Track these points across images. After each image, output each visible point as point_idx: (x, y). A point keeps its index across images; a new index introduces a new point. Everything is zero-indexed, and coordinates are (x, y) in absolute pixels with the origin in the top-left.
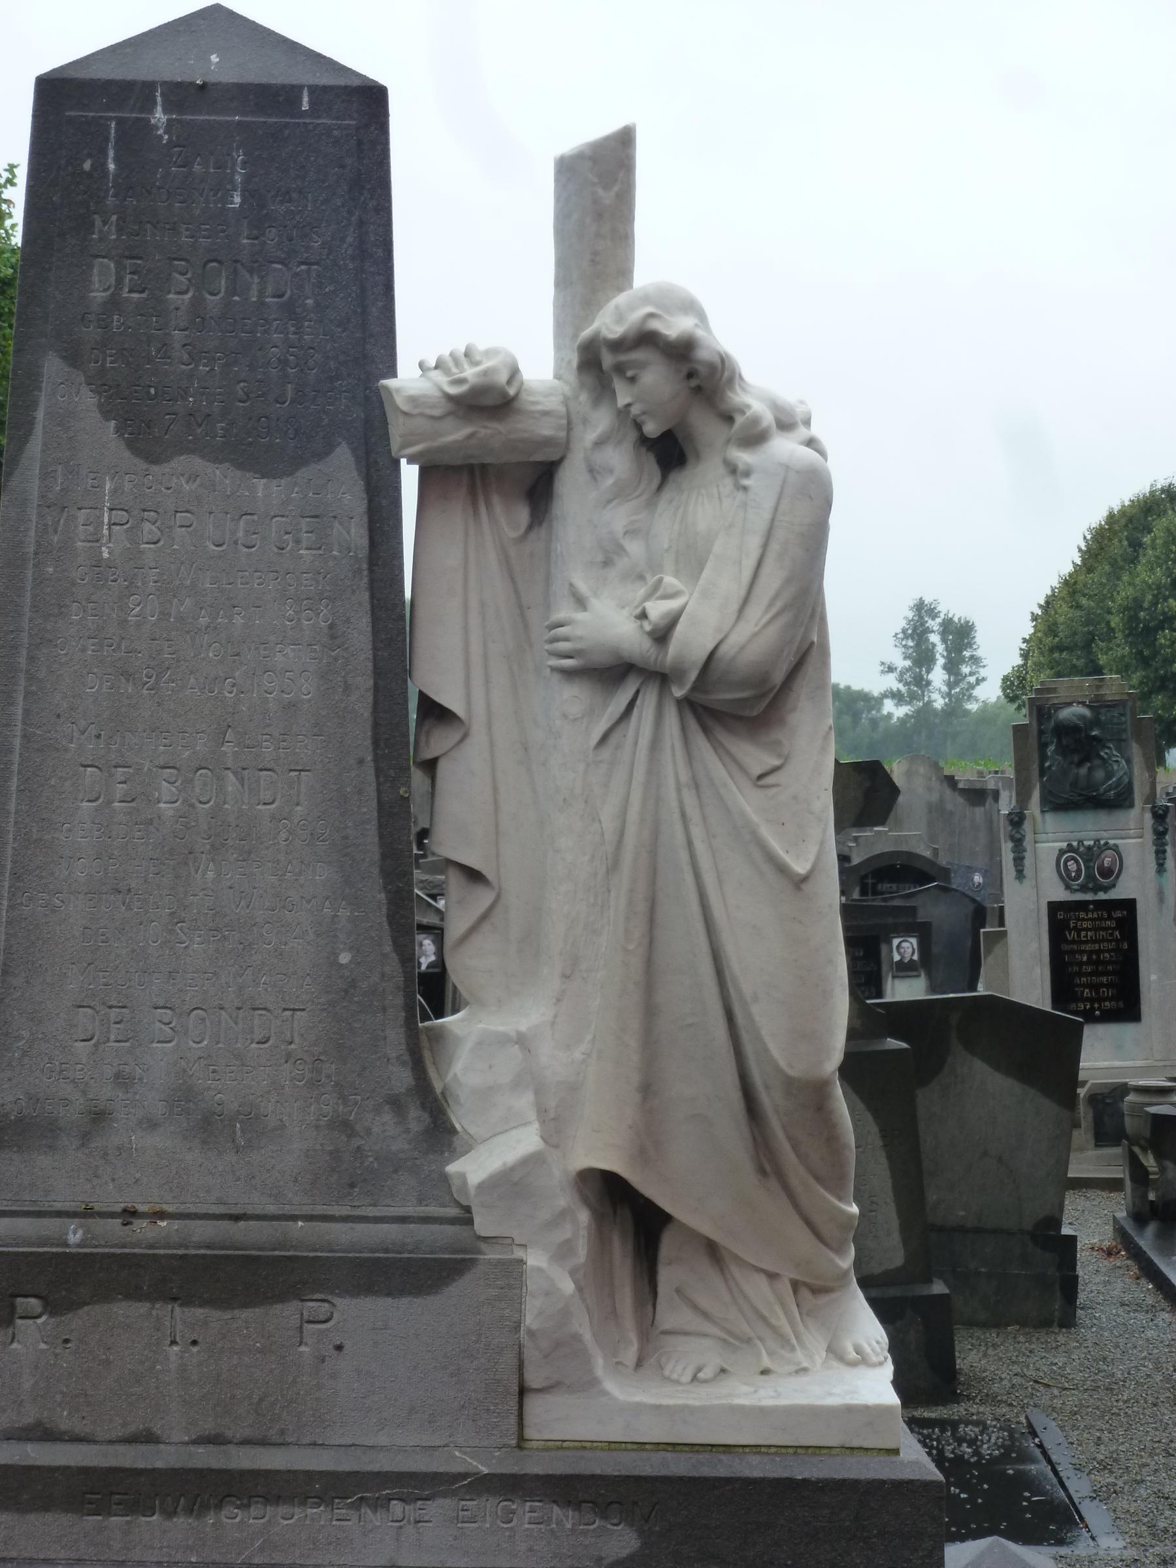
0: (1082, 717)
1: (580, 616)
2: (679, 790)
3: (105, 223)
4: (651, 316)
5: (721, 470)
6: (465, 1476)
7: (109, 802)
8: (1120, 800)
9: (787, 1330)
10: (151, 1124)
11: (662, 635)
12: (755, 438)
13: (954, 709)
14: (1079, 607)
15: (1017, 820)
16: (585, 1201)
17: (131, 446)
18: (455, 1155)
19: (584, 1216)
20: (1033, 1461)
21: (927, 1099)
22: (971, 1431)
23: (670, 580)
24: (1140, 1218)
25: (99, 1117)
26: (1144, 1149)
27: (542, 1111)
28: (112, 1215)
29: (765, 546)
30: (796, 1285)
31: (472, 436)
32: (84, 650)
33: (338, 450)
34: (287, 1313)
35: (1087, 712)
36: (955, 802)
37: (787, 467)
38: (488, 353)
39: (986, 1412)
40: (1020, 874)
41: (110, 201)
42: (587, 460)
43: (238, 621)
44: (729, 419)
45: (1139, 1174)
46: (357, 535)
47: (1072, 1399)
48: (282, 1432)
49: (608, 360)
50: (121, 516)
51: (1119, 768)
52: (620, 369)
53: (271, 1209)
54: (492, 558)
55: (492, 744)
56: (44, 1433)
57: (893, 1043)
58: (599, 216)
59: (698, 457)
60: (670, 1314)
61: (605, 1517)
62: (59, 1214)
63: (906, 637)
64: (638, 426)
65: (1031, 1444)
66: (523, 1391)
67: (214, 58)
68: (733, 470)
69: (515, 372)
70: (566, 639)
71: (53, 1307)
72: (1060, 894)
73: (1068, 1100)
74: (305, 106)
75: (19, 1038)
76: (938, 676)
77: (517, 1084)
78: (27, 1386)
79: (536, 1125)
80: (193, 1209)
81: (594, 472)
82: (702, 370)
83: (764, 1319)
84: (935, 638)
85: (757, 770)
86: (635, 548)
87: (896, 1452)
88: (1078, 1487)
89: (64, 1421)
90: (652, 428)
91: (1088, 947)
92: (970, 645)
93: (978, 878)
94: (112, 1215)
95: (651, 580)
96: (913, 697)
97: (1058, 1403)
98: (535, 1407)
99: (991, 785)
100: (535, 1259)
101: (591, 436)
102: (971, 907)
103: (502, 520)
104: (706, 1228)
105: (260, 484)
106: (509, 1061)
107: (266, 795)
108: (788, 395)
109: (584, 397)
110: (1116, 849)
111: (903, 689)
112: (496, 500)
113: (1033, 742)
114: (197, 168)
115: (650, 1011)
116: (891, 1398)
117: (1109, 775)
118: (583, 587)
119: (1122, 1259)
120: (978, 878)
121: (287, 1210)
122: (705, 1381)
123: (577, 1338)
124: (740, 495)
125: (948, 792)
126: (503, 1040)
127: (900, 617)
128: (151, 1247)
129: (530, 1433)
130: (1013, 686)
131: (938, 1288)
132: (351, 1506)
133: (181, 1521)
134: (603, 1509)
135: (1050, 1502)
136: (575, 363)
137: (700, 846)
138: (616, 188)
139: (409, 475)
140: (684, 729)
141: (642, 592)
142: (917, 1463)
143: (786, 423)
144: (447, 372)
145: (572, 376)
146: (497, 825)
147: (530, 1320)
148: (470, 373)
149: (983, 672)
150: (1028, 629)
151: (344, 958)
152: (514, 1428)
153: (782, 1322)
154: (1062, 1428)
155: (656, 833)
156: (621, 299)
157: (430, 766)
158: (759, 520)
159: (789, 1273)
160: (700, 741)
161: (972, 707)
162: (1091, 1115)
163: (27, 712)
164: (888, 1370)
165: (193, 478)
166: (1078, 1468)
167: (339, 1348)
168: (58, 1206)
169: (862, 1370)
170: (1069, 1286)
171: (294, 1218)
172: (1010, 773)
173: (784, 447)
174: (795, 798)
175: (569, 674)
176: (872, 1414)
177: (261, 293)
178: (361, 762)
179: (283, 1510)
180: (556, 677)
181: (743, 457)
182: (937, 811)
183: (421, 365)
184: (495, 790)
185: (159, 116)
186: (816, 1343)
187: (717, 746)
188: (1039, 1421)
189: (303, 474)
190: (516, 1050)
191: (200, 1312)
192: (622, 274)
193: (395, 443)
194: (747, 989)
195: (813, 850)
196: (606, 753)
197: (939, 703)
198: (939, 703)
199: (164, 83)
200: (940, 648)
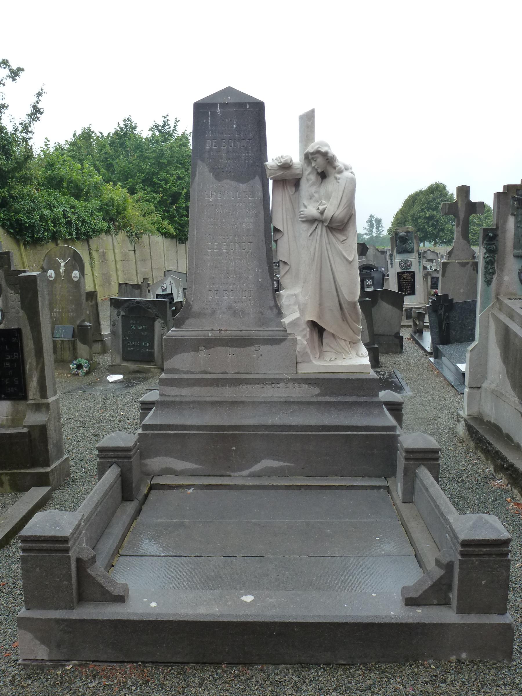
0: (404, 235)
1: (306, 210)
2: (326, 245)
3: (209, 133)
4: (319, 147)
5: (334, 179)
6: (286, 379)
7: (213, 250)
8: (412, 251)
9: (348, 350)
10: (224, 313)
11: (322, 213)
12: (340, 172)
13: (378, 237)
14: (403, 215)
15: (391, 256)
16: (308, 327)
17: (216, 178)
18: (283, 318)
19: (308, 329)
20: (394, 378)
21: (374, 310)
22: (382, 373)
23: (323, 201)
24: (415, 332)
25: (214, 312)
26: (416, 320)
27: (300, 309)
28: (217, 330)
29: (343, 194)
30: (350, 342)
31: (283, 173)
32: (207, 220)
33: (256, 178)
34: (251, 348)
35: (405, 234)
36: (379, 254)
37: (347, 178)
38: (286, 156)
39: (385, 369)
40: (392, 266)
41: (210, 128)
42: (306, 178)
43: (238, 213)
44: (335, 168)
45: (415, 324)
46: (261, 194)
47: (402, 366)
48: (251, 371)
49: (310, 157)
50: (214, 192)
51: (412, 245)
52: (313, 158)
53: (248, 329)
54: (288, 199)
55: (288, 236)
56: (206, 372)
57: (367, 299)
58: (308, 127)
59: (329, 176)
60: (325, 348)
61: (313, 386)
62: (207, 330)
63: (368, 222)
64: (317, 170)
65: (394, 375)
66: (297, 363)
67: (229, 98)
68: (336, 178)
69: (291, 160)
70: (303, 214)
71: (206, 348)
72: (400, 270)
73: (402, 310)
74: (248, 107)
75: (198, 297)
76: (375, 230)
77: (295, 304)
78: (202, 363)
79: (299, 312)
80: (232, 329)
81: (308, 180)
82: (329, 158)
83: (344, 349)
84: (374, 222)
85: (342, 240)
86: (316, 195)
87: (370, 373)
88: (403, 383)
89: (209, 370)
90: (320, 171)
91: (405, 281)
92: (381, 223)
93: (383, 269)
94: (217, 330)
95: (320, 202)
96: (370, 234)
97: (399, 367)
98: (299, 366)
99: (385, 250)
100: (299, 338)
101: (307, 173)
102: (382, 274)
103: (290, 191)
104: (332, 331)
105: (241, 185)
106: (293, 300)
107: (244, 248)
108: (347, 163)
109: (305, 165)
110: (411, 261)
111: (368, 233)
112: (288, 187)
113: (395, 240)
114: (226, 121)
115: (321, 289)
116: (369, 363)
117: (409, 246)
118: (306, 204)
119: (412, 340)
120: (383, 269)
121: (251, 329)
122: (332, 361)
123: (307, 353)
124: (338, 184)
125: (377, 252)
126: (292, 295)
127: (367, 218)
128: (225, 336)
129: (299, 371)
130: (390, 231)
131: (376, 346)
132: (264, 385)
133: (232, 388)
134: (313, 385)
135: (397, 386)
136: (304, 158)
137: (330, 256)
138: (311, 121)
139: (271, 182)
140: (327, 232)
141: (318, 204)
142: (374, 375)
143: (347, 169)
144: (278, 161)
145: (303, 161)
146: (290, 253)
147: (298, 349)
148: (282, 160)
149: (383, 229)
150: (392, 220)
151: (260, 280)
152: (295, 370)
153: (347, 349)
154: (400, 372)
155: (321, 254)
156: (313, 144)
157: (276, 241)
158: (341, 189)
159: (349, 340)
160: (330, 234)
161: (381, 236)
162: (405, 314)
163: (197, 233)
164: (368, 358)
165: (228, 184)
166: (403, 379)
167: (261, 355)
168: (207, 329)
169: (363, 358)
170: (401, 346)
171: (252, 331)
172: (390, 248)
173: (346, 174)
174: (349, 245)
175: (304, 222)
176: (365, 366)
177: (240, 146)
178: (262, 241)
179: (251, 386)
180: (301, 222)
181: (338, 176)
182: (375, 256)
183: (273, 160)
184: (289, 246)
185: (219, 110)
186: (354, 353)
187: (334, 235)
188: (395, 371)
189: (250, 182)
190: (294, 297)
191: (235, 349)
192: (313, 139)
193: (268, 175)
194: (340, 284)
195: (353, 256)
196: (311, 238)
197: (375, 235)
198: (375, 235)
199: (219, 103)
200: (375, 224)
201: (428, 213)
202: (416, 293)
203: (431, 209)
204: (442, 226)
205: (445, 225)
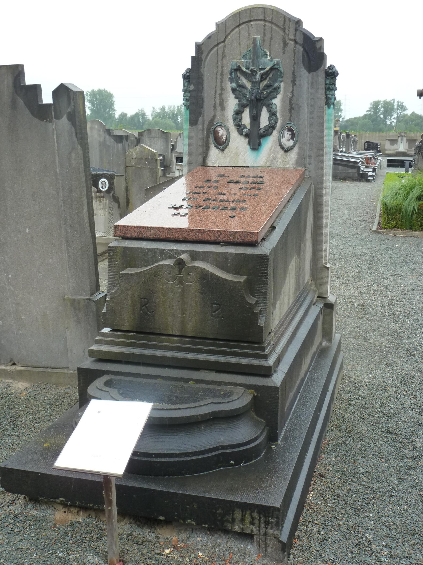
36: (110, 141)
125: (107, 137)
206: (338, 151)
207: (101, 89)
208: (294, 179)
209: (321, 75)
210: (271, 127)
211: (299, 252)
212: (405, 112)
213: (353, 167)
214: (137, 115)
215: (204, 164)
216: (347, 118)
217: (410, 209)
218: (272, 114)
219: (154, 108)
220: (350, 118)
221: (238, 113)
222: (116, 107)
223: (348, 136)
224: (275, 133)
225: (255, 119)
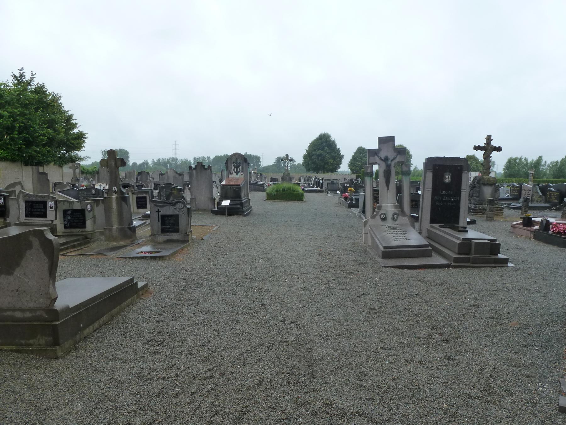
36: (177, 176)
125: (176, 174)
201: (318, 152)
202: (148, 208)
203: (320, 149)
204: (326, 160)
205: (329, 160)
206: (256, 181)
207: (121, 148)
208: (243, 179)
209: (247, 163)
210: (239, 171)
211: (245, 189)
212: (295, 163)
213: (262, 186)
214: (143, 164)
215: (229, 177)
216: (264, 165)
217: (274, 194)
218: (240, 169)
219: (153, 160)
220: (265, 165)
221: (234, 169)
222: (130, 159)
223: (261, 175)
224: (240, 172)
225: (237, 170)
